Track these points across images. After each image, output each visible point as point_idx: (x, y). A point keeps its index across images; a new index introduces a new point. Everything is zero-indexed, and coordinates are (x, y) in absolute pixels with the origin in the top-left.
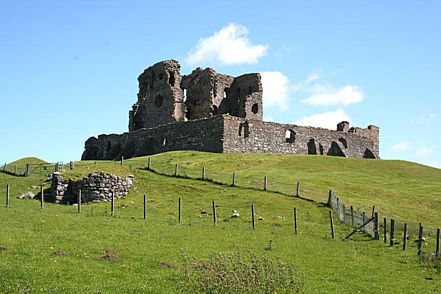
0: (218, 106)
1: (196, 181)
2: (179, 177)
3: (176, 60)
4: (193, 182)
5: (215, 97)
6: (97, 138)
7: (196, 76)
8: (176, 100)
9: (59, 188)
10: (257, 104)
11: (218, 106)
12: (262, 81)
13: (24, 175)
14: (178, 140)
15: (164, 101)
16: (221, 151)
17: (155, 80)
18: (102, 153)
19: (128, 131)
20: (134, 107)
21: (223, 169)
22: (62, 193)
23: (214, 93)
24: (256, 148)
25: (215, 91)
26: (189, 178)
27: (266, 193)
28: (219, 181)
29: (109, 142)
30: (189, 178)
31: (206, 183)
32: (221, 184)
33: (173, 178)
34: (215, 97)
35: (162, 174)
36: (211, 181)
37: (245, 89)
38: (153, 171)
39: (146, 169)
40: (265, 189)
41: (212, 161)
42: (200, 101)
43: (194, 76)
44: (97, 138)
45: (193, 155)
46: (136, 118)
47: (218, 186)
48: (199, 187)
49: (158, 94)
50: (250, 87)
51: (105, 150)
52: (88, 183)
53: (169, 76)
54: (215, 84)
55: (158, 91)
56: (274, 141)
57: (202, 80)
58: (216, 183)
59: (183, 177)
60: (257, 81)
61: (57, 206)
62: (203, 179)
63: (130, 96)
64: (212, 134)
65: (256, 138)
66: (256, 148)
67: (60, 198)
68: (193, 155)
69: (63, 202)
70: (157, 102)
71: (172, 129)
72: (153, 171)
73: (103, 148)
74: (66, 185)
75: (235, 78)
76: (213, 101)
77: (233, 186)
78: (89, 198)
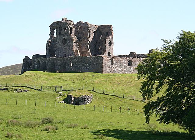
0: (91, 41)
1: (112, 96)
2: (105, 94)
3: (72, 21)
4: (111, 96)
5: (90, 37)
6: (31, 58)
7: (79, 25)
8: (74, 42)
9: (72, 100)
10: (111, 42)
11: (91, 41)
12: (113, 29)
13: (40, 90)
14: (79, 64)
15: (67, 41)
16: (102, 73)
17: (59, 27)
18: (34, 66)
19: (45, 54)
20: (48, 41)
21: (109, 84)
22: (73, 101)
23: (90, 35)
24: (116, 70)
25: (90, 34)
26: (108, 95)
27: (134, 101)
28: (119, 96)
29: (39, 61)
30: (108, 95)
31: (115, 97)
32: (120, 97)
33: (103, 95)
34: (90, 37)
35: (99, 93)
36: (116, 96)
37: (104, 32)
38: (95, 92)
39: (92, 91)
40: (134, 99)
41: (103, 80)
42: (82, 39)
43: (78, 25)
44: (31, 58)
45: (93, 76)
46: (51, 46)
47: (119, 98)
48: (113, 98)
49: (64, 38)
50: (107, 32)
51: (36, 64)
52: (82, 98)
53: (70, 30)
54: (90, 31)
55: (64, 36)
56: (123, 66)
57: (82, 28)
58: (118, 97)
59: (106, 94)
60: (111, 30)
61: (72, 105)
62: (113, 95)
63: (45, 36)
64: (97, 64)
65: (116, 65)
66: (116, 70)
67: (73, 103)
68: (93, 76)
69: (74, 104)
70: (63, 41)
71: (76, 59)
72: (95, 92)
73: (35, 63)
74: (74, 99)
75: (98, 26)
76: (89, 40)
77: (123, 98)
78: (83, 103)
